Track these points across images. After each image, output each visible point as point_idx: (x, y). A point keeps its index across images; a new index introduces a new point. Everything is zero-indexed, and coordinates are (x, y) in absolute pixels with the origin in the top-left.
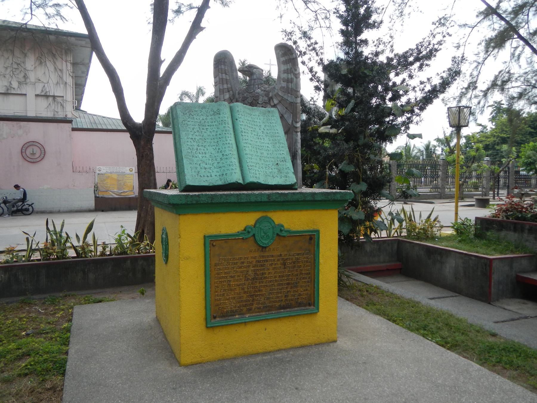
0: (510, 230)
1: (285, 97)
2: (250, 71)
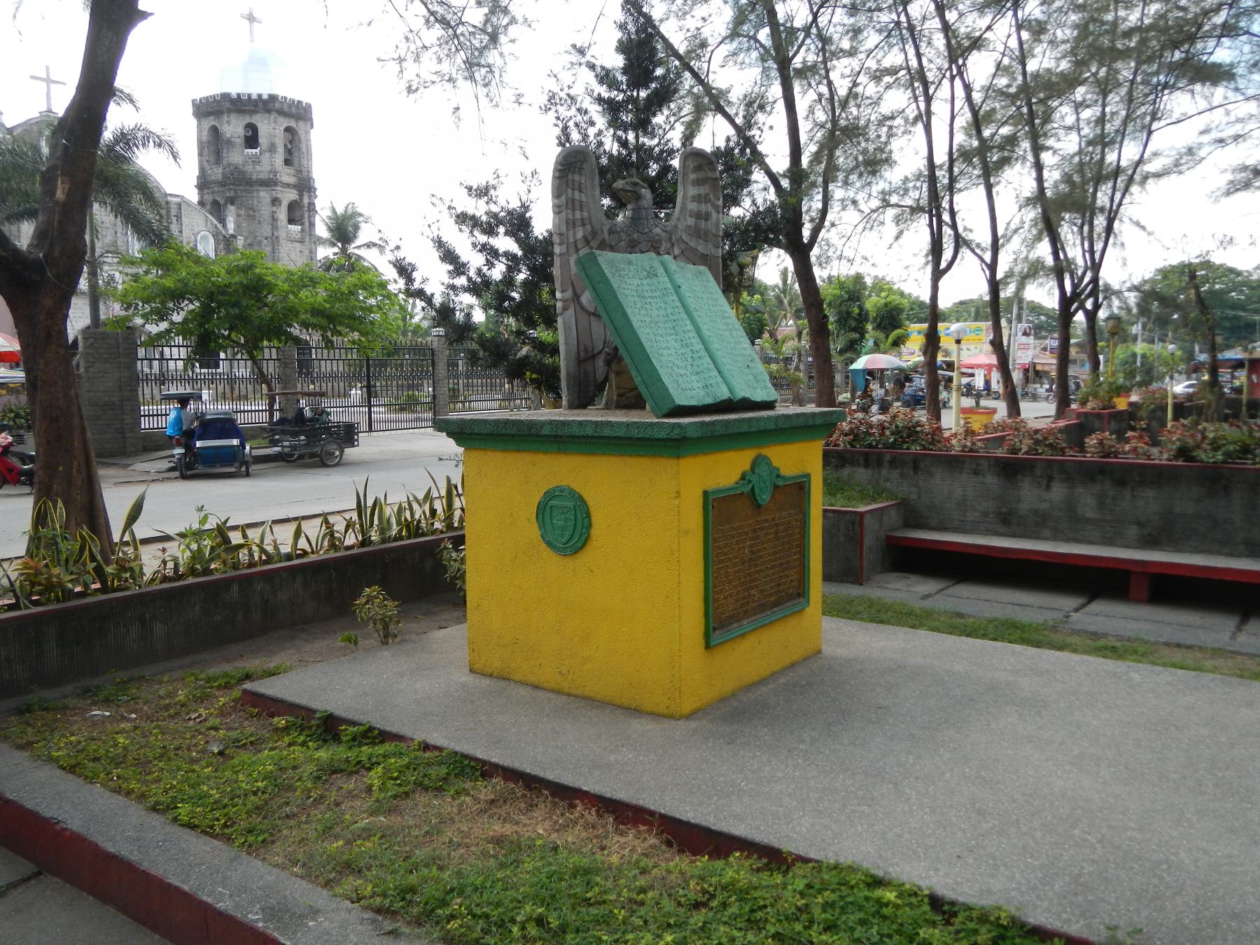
0: (859, 465)
1: (692, 244)
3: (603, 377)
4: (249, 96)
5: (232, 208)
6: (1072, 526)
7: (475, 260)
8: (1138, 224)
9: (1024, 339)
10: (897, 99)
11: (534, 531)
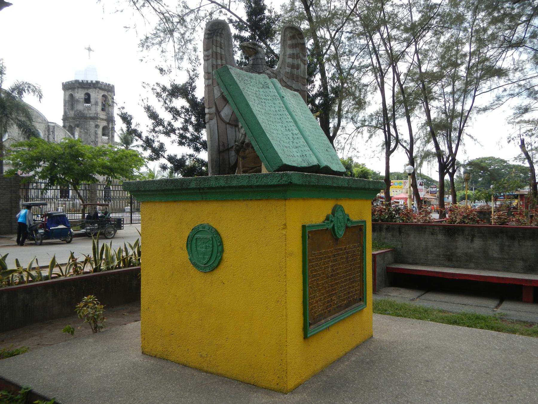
2: (255, 49)
3: (234, 162)
4: (87, 81)
5: (77, 129)
6: (486, 260)
7: (166, 116)
8: (470, 136)
10: (368, 78)
11: (184, 255)
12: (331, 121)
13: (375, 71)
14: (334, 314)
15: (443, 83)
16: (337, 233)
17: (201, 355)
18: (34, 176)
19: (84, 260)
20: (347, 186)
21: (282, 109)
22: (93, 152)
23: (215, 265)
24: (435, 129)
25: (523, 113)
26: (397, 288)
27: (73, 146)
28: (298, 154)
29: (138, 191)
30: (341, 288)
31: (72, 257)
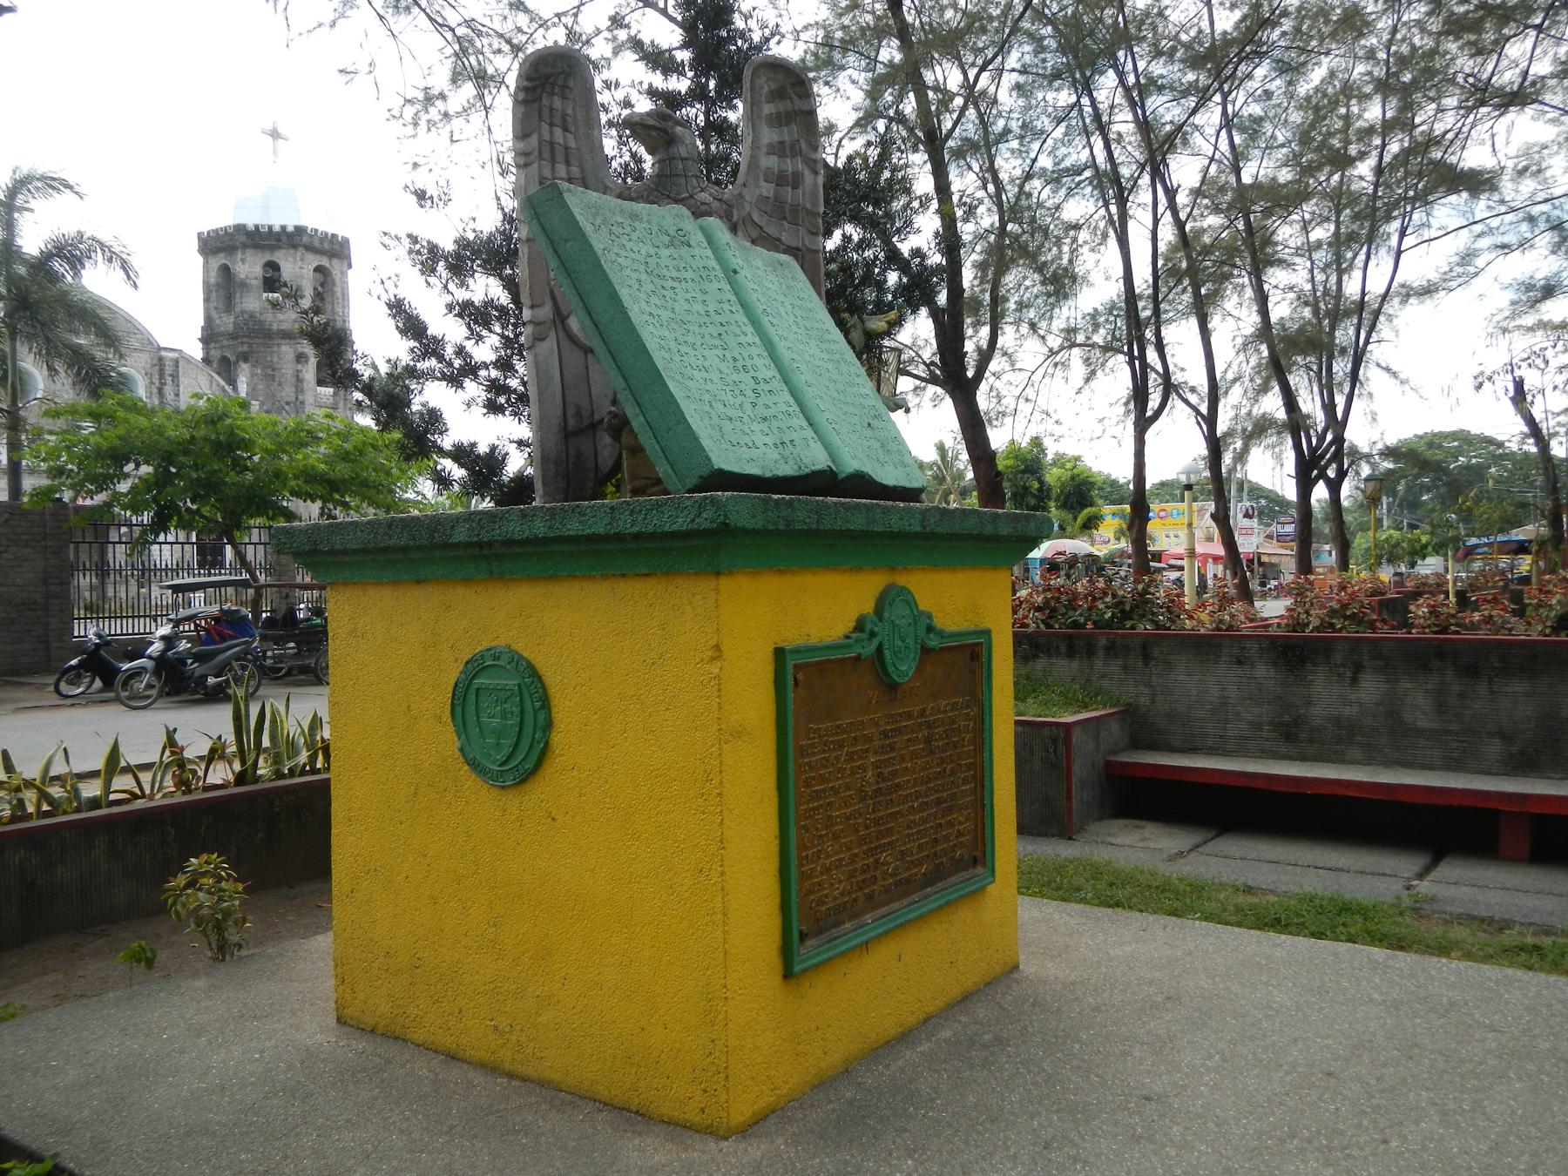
0: (1058, 653)
2: (665, 131)
3: (610, 463)
4: (270, 227)
5: (245, 366)
6: (1393, 739)
7: (452, 331)
8: (1388, 369)
9: (1246, 522)
10: (1081, 207)
11: (447, 739)
12: (969, 332)
13: (1100, 182)
14: (887, 903)
15: (1307, 216)
16: (891, 669)
17: (496, 1028)
18: (108, 505)
19: (205, 752)
20: (919, 529)
21: (726, 306)
22: (278, 435)
23: (528, 766)
24: (1281, 351)
25: (1537, 301)
26: (1135, 822)
27: (220, 418)
28: (769, 440)
29: (314, 552)
30: (909, 827)
31: (171, 742)
